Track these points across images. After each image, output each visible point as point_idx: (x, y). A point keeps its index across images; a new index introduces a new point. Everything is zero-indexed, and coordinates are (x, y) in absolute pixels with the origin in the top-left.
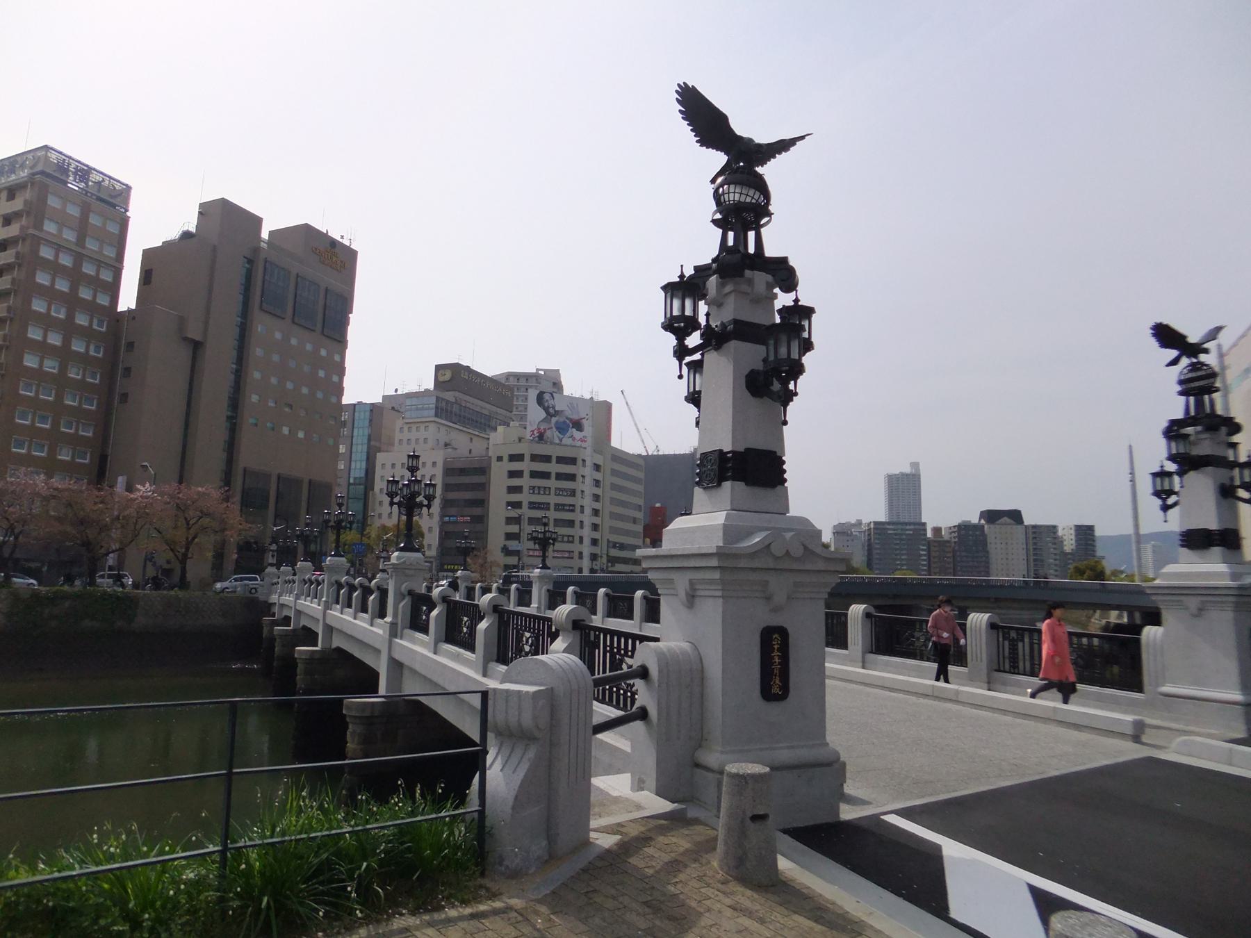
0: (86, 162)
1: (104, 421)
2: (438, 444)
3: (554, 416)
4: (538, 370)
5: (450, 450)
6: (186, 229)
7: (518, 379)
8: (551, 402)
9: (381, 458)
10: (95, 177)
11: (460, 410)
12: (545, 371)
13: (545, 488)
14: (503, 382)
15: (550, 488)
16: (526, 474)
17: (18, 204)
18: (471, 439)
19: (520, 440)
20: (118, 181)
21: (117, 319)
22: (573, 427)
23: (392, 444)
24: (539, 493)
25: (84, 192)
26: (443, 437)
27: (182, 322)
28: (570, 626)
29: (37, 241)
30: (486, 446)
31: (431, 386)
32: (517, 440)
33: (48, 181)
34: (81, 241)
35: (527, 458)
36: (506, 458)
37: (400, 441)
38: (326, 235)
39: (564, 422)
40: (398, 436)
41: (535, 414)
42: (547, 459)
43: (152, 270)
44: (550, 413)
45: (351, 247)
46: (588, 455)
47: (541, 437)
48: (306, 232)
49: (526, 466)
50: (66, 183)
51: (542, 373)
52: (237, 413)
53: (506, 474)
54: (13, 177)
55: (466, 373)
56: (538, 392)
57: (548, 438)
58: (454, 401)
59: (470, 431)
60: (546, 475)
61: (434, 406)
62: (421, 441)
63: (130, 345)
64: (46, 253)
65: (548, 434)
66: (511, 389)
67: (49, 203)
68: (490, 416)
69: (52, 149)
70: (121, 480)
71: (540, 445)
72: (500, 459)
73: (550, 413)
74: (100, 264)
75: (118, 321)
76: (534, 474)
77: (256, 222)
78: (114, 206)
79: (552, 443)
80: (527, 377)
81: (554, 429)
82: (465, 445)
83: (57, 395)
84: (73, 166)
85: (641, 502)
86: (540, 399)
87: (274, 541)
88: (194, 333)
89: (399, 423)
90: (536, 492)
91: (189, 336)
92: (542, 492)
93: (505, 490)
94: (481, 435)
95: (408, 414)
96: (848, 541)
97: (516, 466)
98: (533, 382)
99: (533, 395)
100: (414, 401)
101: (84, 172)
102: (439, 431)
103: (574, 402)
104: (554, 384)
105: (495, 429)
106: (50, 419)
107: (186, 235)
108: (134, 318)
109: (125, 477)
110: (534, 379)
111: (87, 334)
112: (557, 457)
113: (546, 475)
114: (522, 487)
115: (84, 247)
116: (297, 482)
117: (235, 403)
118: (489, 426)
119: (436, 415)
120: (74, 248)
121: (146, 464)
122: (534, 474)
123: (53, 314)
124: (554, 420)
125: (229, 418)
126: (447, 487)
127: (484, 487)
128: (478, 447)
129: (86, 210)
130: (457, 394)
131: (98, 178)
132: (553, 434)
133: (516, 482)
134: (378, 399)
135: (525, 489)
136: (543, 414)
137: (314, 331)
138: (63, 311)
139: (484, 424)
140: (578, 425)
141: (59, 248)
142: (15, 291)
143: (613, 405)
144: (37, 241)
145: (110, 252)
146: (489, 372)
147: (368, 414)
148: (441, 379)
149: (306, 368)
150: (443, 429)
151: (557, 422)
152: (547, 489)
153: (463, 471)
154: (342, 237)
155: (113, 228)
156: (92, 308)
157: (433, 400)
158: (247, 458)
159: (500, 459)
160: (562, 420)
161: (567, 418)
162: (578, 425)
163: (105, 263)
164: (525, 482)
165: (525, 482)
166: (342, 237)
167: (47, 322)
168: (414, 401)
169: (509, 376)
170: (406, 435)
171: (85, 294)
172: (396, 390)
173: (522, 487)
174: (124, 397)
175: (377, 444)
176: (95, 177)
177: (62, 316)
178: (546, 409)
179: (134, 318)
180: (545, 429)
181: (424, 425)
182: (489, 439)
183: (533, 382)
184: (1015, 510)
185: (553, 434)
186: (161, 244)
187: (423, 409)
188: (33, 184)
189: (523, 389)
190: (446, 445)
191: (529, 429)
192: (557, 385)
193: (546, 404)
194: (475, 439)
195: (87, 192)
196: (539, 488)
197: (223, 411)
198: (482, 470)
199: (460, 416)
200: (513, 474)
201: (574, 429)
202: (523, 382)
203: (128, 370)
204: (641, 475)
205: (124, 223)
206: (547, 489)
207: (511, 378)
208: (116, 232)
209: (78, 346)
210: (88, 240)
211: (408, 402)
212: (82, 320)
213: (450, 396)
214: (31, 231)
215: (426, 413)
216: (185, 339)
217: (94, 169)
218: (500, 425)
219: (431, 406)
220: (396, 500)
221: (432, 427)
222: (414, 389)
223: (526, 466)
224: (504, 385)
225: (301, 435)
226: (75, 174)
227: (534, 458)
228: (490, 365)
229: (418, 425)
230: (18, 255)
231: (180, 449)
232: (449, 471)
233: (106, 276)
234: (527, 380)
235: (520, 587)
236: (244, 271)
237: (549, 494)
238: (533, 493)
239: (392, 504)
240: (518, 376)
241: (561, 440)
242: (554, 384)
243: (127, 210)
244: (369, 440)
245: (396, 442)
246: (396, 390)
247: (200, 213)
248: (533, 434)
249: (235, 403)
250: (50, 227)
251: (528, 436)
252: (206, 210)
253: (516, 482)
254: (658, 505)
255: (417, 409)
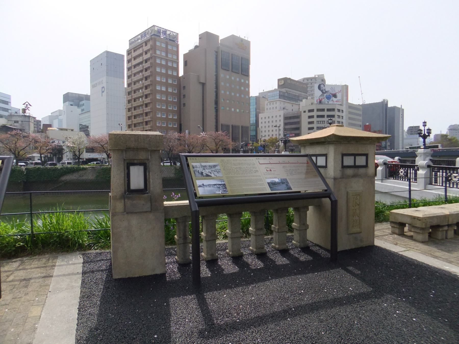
0: (165, 28)
1: (180, 113)
2: (281, 109)
3: (325, 93)
4: (315, 75)
5: (285, 110)
6: (196, 45)
7: (311, 80)
8: (324, 88)
9: (260, 116)
10: (168, 33)
11: (288, 95)
12: (318, 75)
13: (323, 121)
14: (302, 82)
15: (325, 121)
16: (315, 117)
17: (148, 47)
18: (293, 105)
19: (312, 104)
20: (175, 32)
21: (179, 79)
22: (333, 97)
23: (264, 110)
24: (320, 123)
25: (165, 38)
26: (283, 106)
27: (198, 77)
28: (427, 167)
29: (155, 57)
30: (298, 108)
31: (277, 88)
32: (311, 104)
33: (156, 37)
34: (167, 55)
35: (315, 110)
36: (307, 111)
37: (267, 109)
38: (239, 38)
39: (329, 95)
40: (266, 107)
41: (318, 93)
42: (323, 110)
43: (187, 61)
44: (324, 92)
45: (248, 40)
46: (344, 108)
47: (320, 102)
48: (233, 37)
49: (315, 113)
50: (160, 36)
51: (317, 76)
52: (217, 106)
53: (307, 117)
54: (146, 38)
55: (289, 81)
56: (318, 85)
57: (323, 102)
58: (285, 92)
59: (292, 102)
60: (323, 116)
61: (279, 95)
62: (275, 108)
63: (184, 87)
64: (158, 61)
65: (323, 100)
66: (307, 84)
67: (157, 44)
68: (299, 96)
69: (155, 26)
70: (187, 131)
71: (320, 105)
72: (305, 112)
73: (324, 92)
74: (173, 62)
75: (179, 80)
76: (318, 116)
77: (217, 37)
78: (174, 41)
79: (325, 104)
80: (311, 79)
81: (325, 98)
82: (291, 108)
83: (166, 107)
84: (162, 30)
85: (361, 123)
86: (319, 88)
87: (242, 147)
88: (202, 81)
89: (266, 102)
90: (319, 123)
91: (202, 81)
92: (322, 123)
93: (307, 123)
94: (296, 103)
95: (269, 99)
96: (456, 133)
97: (311, 114)
98: (313, 81)
99: (316, 86)
100: (271, 94)
101: (165, 32)
102: (293, 106)
103: (333, 87)
104: (322, 80)
105: (301, 101)
106: (165, 114)
107: (196, 47)
108: (184, 78)
109: (188, 130)
110: (314, 79)
111: (172, 85)
112: (327, 109)
113: (323, 116)
114: (314, 122)
115: (168, 57)
116: (238, 127)
117: (217, 103)
118: (299, 100)
119: (280, 98)
120: (165, 58)
121: (199, 126)
122: (318, 116)
123: (162, 81)
124: (325, 95)
125: (215, 108)
126: (285, 124)
127: (299, 123)
128: (295, 108)
129: (167, 44)
130: (287, 89)
131: (169, 33)
132: (325, 100)
133: (311, 120)
134: (257, 95)
135: (315, 122)
136: (320, 93)
137: (239, 73)
138: (165, 79)
139: (296, 99)
140: (335, 96)
141: (161, 59)
142: (152, 75)
143: (349, 86)
144: (155, 57)
145: (175, 57)
146: (296, 79)
147: (255, 100)
148: (280, 84)
149: (238, 87)
150: (282, 103)
151: (326, 96)
152: (323, 122)
153: (290, 118)
154: (245, 37)
155: (175, 49)
156: (172, 77)
157: (278, 92)
158: (223, 120)
159: (305, 112)
160: (328, 94)
161: (330, 93)
162: (335, 96)
163: (174, 61)
164: (315, 119)
165: (315, 119)
166: (245, 37)
167: (161, 83)
168: (271, 94)
169: (304, 79)
170: (269, 107)
171: (170, 73)
172: (263, 90)
173: (314, 122)
174: (184, 105)
175: (259, 111)
176: (168, 33)
177: (165, 81)
178: (322, 91)
179: (184, 78)
180: (322, 99)
181: (272, 102)
182: (300, 105)
183: (313, 81)
184: (216, 35)
185: (325, 100)
186: (188, 52)
187: (275, 96)
188: (152, 39)
189: (310, 84)
190: (284, 109)
191: (315, 99)
192: (323, 80)
193: (322, 89)
194: (294, 105)
195: (166, 38)
196: (320, 121)
197: (213, 106)
198: (298, 117)
199: (288, 97)
200: (310, 117)
201: (333, 98)
202: (310, 81)
203: (184, 96)
204: (361, 113)
205: (177, 46)
206: (319, 122)
207: (305, 80)
208: (176, 50)
209: (170, 90)
210: (169, 54)
211: (269, 94)
212: (170, 81)
213: (284, 90)
214: (153, 55)
215: (276, 97)
216: (200, 83)
217: (168, 30)
218: (303, 99)
219: (277, 95)
220: (283, 141)
221: (278, 103)
222: (271, 89)
223: (315, 113)
224: (303, 83)
225: (238, 110)
226: (163, 33)
227: (318, 110)
228: (297, 76)
229: (276, 102)
230: (151, 63)
231: (201, 119)
232: (285, 118)
233: (175, 66)
234: (311, 80)
235: (400, 158)
236: (215, 56)
237: (325, 123)
238: (318, 123)
239: (282, 142)
240: (308, 79)
241: (328, 102)
242: (322, 80)
243: (178, 42)
244: (256, 110)
245: (266, 109)
246: (263, 90)
247: (200, 38)
248: (317, 101)
249: (217, 103)
250: (158, 52)
251: (315, 102)
252: (201, 37)
253: (311, 120)
254: (367, 124)
255: (272, 96)
